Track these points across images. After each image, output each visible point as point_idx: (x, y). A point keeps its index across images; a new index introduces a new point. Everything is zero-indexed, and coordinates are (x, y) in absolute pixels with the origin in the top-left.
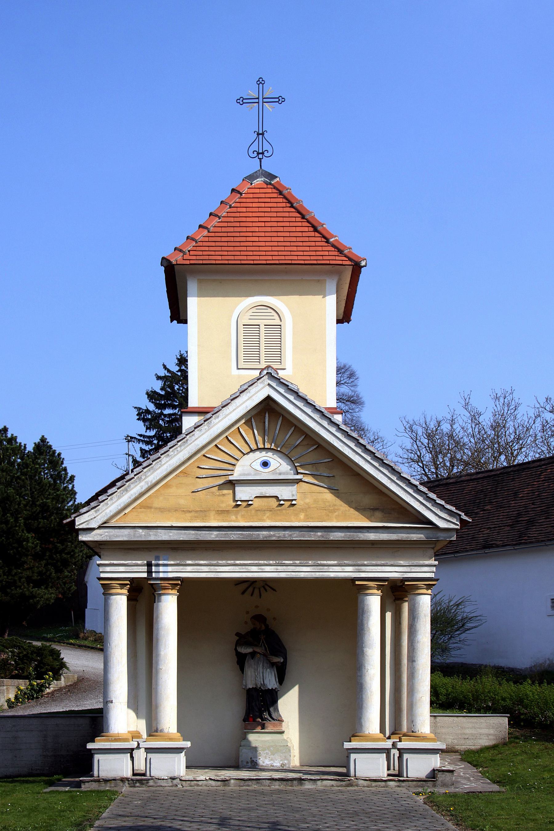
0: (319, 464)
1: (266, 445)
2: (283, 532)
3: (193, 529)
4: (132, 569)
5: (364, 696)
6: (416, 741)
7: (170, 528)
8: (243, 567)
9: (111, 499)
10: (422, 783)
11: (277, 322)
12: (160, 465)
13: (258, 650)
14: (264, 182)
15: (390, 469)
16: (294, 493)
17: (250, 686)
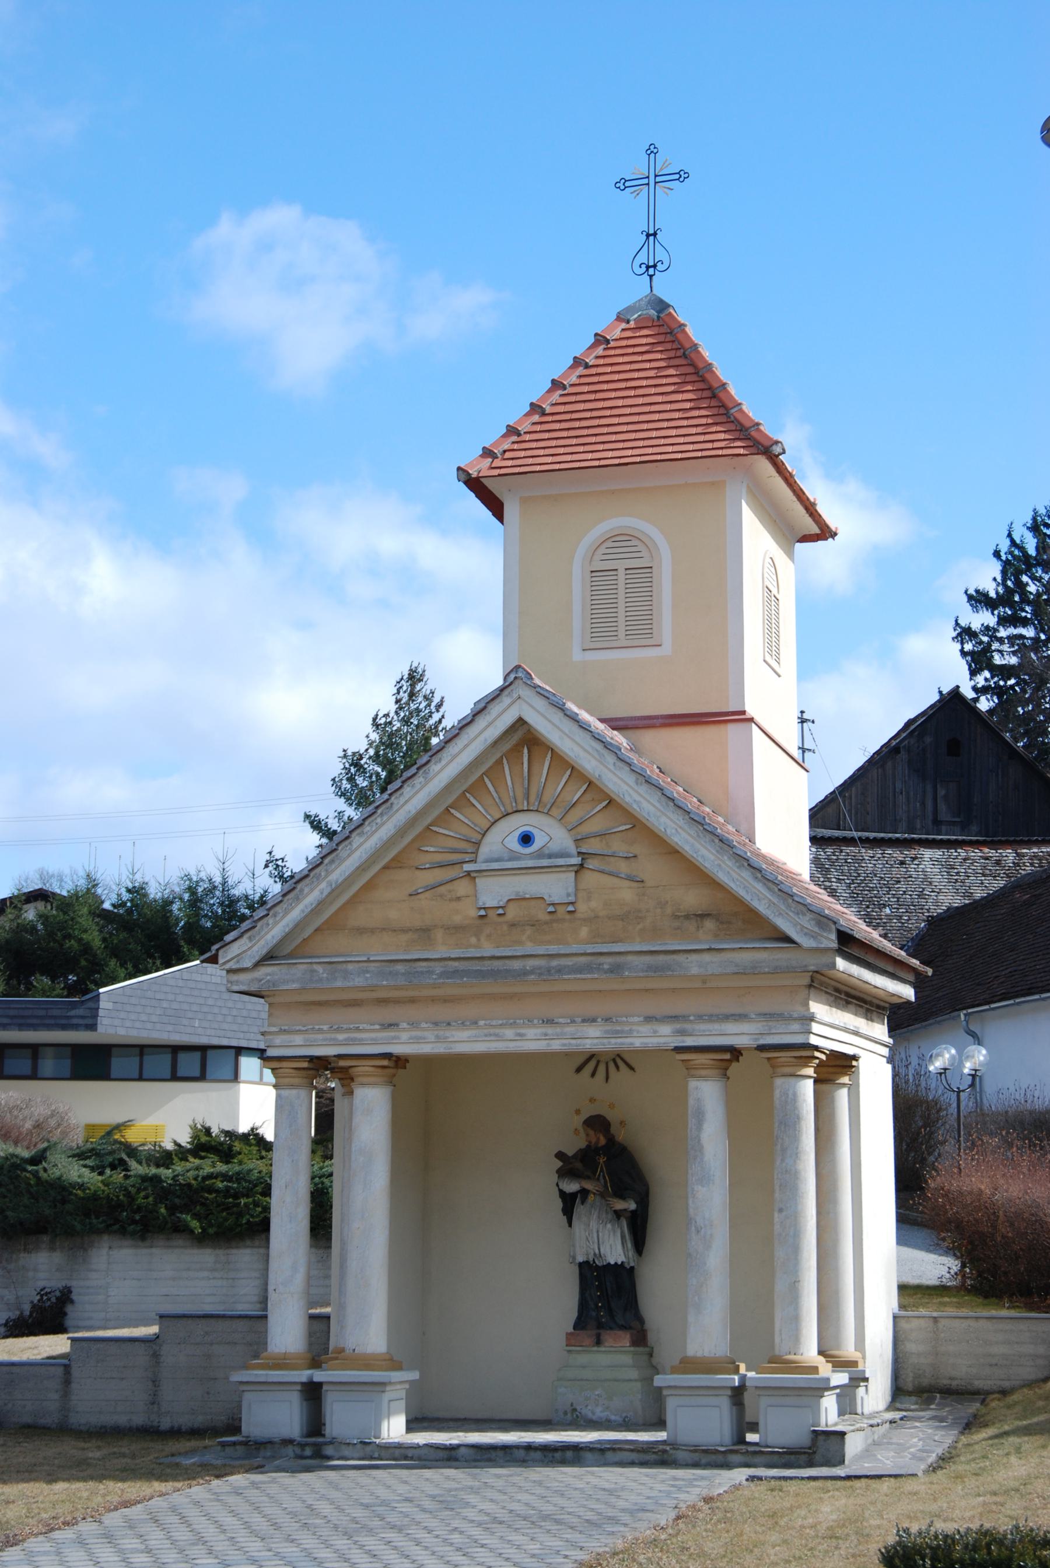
0: (613, 835)
12: (348, 852)
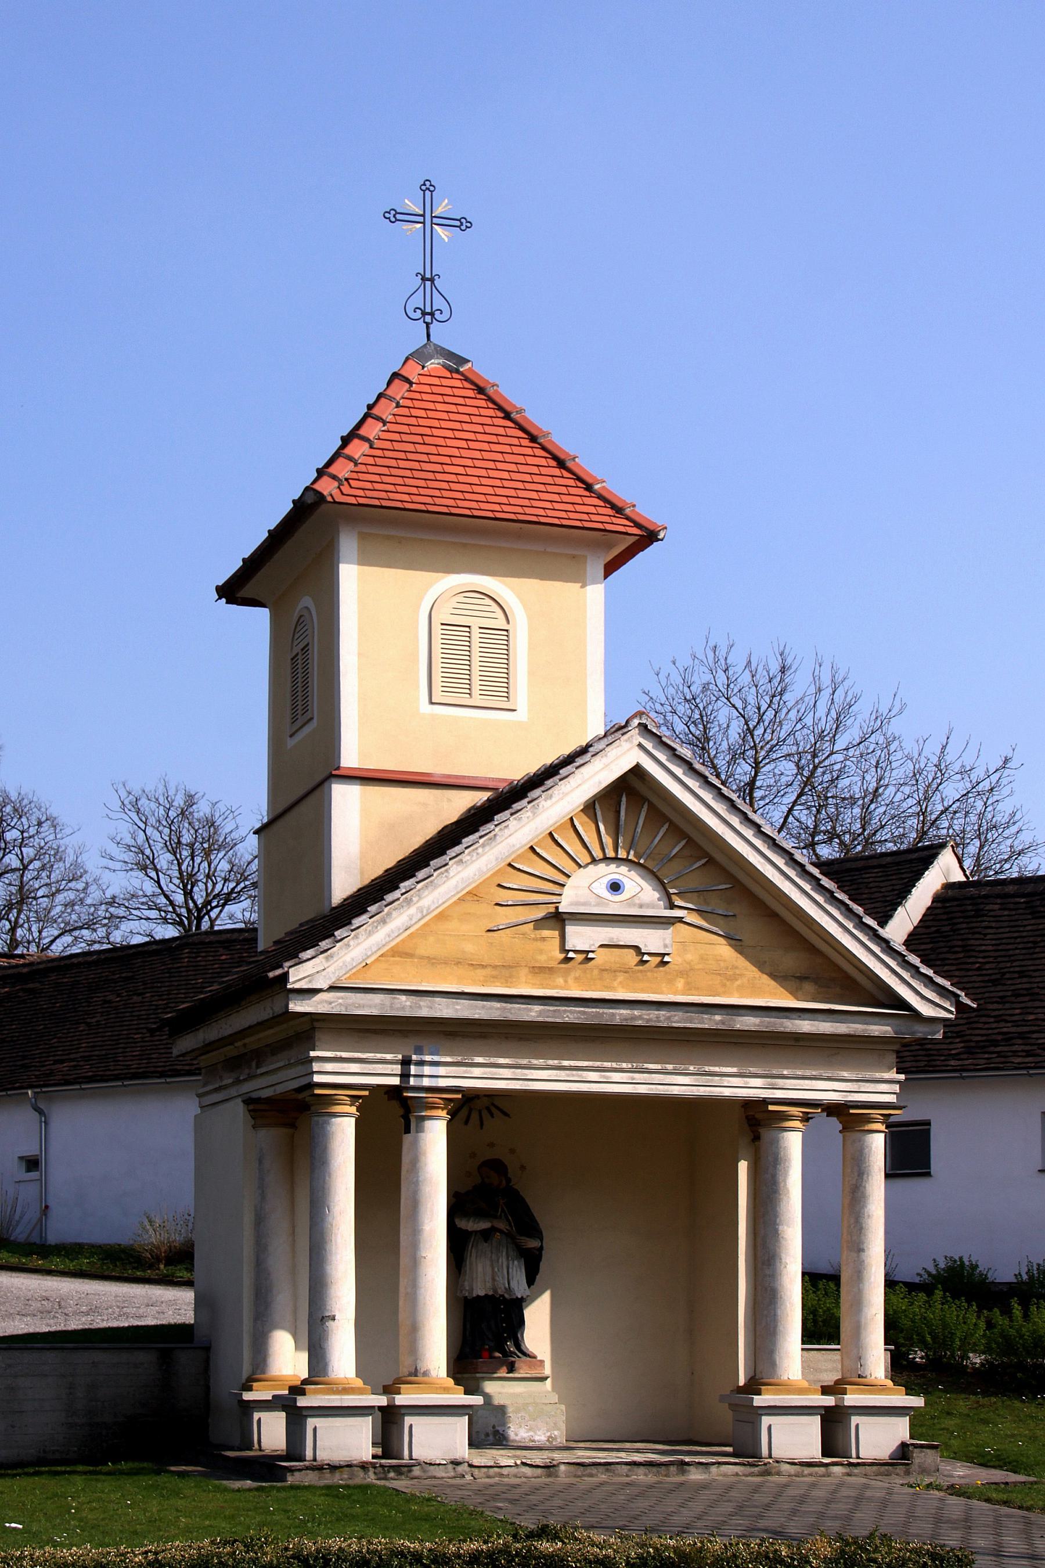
0: (710, 893)
1: (619, 852)
2: (656, 1012)
3: (497, 999)
4: (374, 1069)
5: (779, 1312)
6: (871, 1392)
7: (456, 996)
8: (574, 1072)
9: (356, 937)
10: (887, 1467)
11: (501, 623)
13: (501, 1225)
14: (443, 366)
15: (843, 908)
16: (668, 942)
17: (480, 1290)
